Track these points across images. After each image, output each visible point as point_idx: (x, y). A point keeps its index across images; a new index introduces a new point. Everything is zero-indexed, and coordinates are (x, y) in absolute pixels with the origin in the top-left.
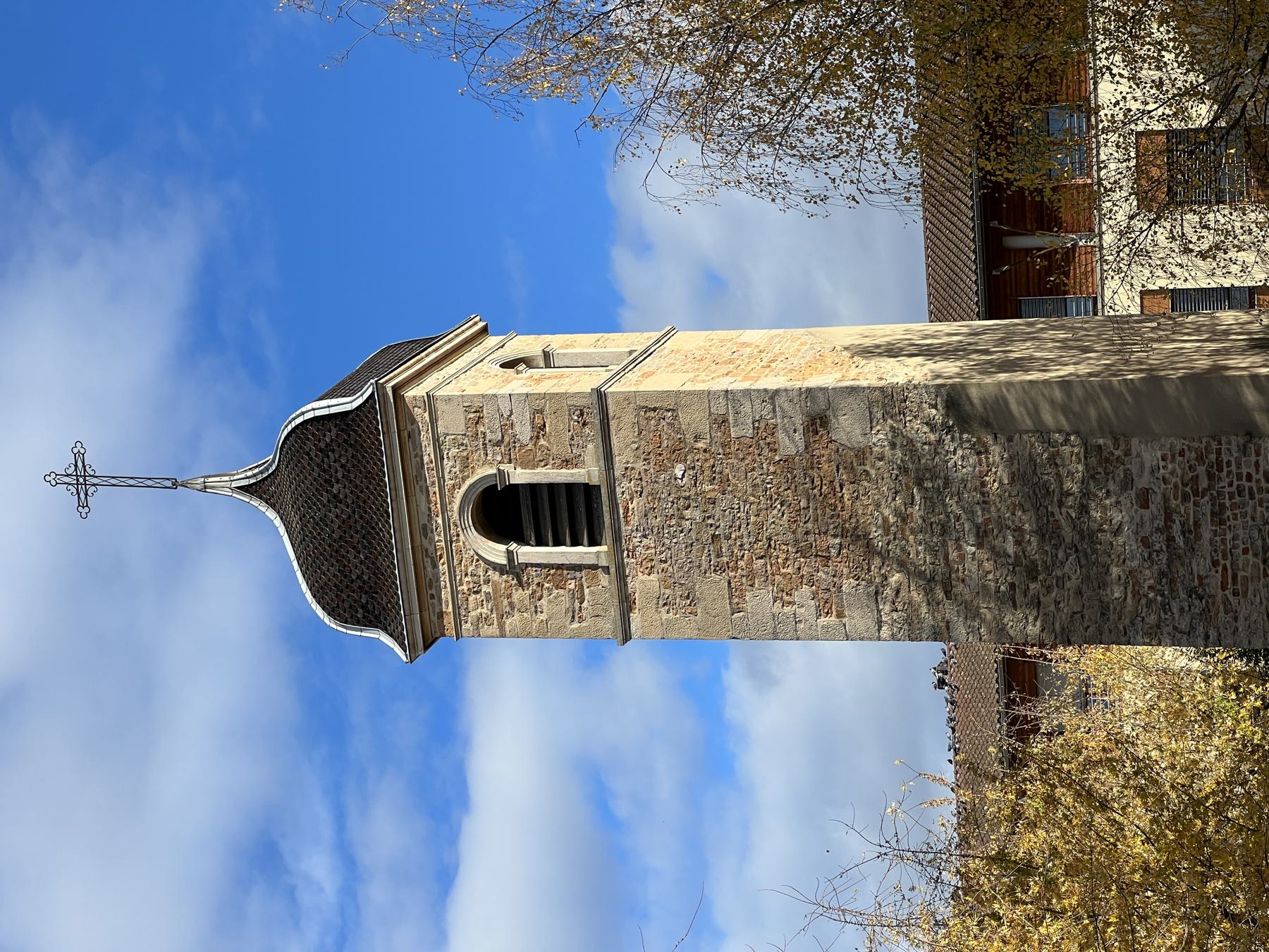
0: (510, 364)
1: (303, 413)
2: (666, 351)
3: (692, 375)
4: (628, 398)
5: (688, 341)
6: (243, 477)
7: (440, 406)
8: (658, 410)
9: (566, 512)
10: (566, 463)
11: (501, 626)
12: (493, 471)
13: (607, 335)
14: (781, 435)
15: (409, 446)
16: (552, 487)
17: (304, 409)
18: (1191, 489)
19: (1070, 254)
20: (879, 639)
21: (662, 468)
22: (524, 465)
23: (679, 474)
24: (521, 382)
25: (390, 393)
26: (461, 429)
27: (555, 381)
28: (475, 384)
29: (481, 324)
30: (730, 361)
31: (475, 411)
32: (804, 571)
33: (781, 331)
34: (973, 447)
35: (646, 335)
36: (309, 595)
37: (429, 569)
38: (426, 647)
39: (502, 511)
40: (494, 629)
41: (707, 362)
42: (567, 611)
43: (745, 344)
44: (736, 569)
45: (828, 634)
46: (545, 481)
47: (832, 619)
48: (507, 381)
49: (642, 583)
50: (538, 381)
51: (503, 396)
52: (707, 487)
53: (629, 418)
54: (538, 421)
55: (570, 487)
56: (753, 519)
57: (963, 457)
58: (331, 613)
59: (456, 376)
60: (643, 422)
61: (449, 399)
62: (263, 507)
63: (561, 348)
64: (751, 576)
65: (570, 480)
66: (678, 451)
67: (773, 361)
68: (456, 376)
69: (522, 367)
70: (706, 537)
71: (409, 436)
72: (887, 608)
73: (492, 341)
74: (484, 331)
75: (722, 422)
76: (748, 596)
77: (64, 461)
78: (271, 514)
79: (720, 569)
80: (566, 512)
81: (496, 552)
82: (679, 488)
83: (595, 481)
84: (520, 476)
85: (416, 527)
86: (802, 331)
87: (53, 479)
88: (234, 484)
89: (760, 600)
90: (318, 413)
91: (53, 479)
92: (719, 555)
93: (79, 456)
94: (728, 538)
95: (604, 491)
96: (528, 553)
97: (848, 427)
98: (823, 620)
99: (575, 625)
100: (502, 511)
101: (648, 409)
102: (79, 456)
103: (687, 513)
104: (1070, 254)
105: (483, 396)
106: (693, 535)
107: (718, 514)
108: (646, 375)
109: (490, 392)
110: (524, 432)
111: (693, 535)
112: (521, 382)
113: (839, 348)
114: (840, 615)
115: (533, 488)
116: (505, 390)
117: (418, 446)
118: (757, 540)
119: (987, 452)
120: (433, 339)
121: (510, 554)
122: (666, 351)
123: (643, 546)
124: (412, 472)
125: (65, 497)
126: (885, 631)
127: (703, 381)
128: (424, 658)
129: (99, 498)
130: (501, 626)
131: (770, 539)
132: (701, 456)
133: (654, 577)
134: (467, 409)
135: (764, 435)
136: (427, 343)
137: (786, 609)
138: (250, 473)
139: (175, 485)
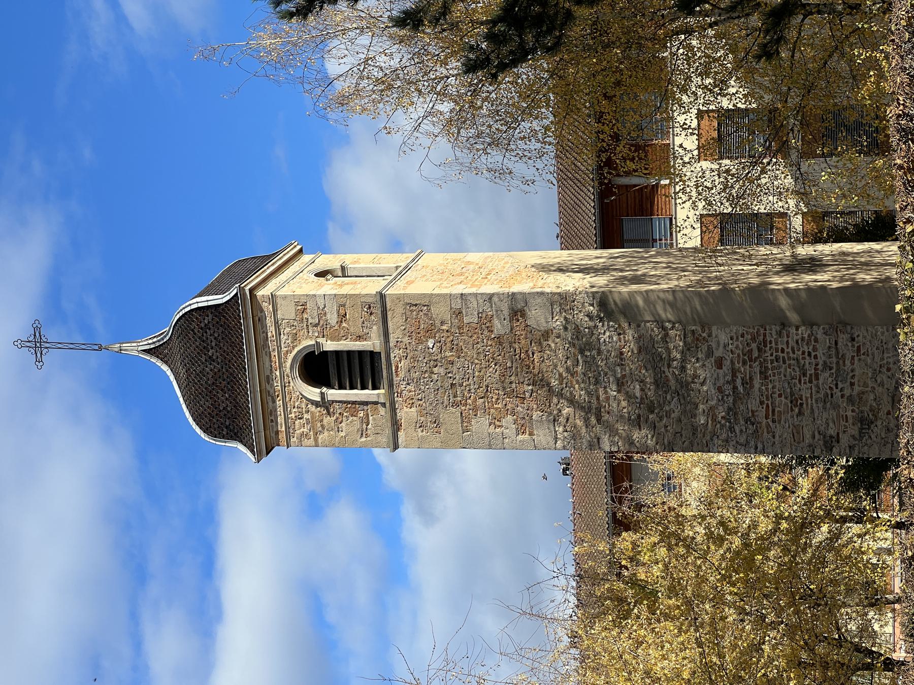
2: (419, 267)
3: (439, 283)
4: (399, 297)
5: (432, 259)
6: (146, 343)
7: (279, 301)
8: (418, 306)
9: (361, 368)
10: (359, 338)
11: (316, 440)
12: (313, 342)
15: (259, 326)
16: (349, 353)
17: (191, 302)
21: (420, 342)
27: (352, 286)
29: (299, 247)
31: (302, 306)
32: (509, 406)
33: (491, 254)
38: (268, 453)
39: (318, 368)
41: (445, 276)
42: (358, 430)
43: (469, 263)
44: (466, 405)
49: (406, 413)
50: (341, 286)
52: (448, 354)
53: (400, 310)
54: (342, 312)
55: (361, 353)
56: (477, 374)
59: (287, 282)
60: (408, 313)
61: (285, 297)
64: (475, 409)
66: (430, 331)
67: (488, 274)
71: (259, 321)
72: (561, 429)
73: (306, 258)
74: (301, 251)
78: (165, 368)
80: (361, 368)
81: (313, 393)
83: (377, 350)
84: (329, 346)
88: (140, 348)
89: (481, 424)
90: (200, 305)
94: (461, 385)
95: (383, 355)
96: (333, 394)
97: (537, 317)
99: (363, 439)
100: (318, 368)
101: (411, 305)
104: (799, 308)
105: (307, 296)
106: (439, 383)
108: (410, 283)
109: (311, 293)
110: (333, 318)
112: (330, 287)
114: (531, 434)
115: (337, 353)
119: (624, 333)
121: (322, 394)
122: (419, 267)
123: (406, 390)
125: (28, 356)
130: (316, 440)
132: (445, 334)
133: (413, 409)
136: (266, 259)
137: (498, 430)
138: (150, 341)
139: (100, 349)
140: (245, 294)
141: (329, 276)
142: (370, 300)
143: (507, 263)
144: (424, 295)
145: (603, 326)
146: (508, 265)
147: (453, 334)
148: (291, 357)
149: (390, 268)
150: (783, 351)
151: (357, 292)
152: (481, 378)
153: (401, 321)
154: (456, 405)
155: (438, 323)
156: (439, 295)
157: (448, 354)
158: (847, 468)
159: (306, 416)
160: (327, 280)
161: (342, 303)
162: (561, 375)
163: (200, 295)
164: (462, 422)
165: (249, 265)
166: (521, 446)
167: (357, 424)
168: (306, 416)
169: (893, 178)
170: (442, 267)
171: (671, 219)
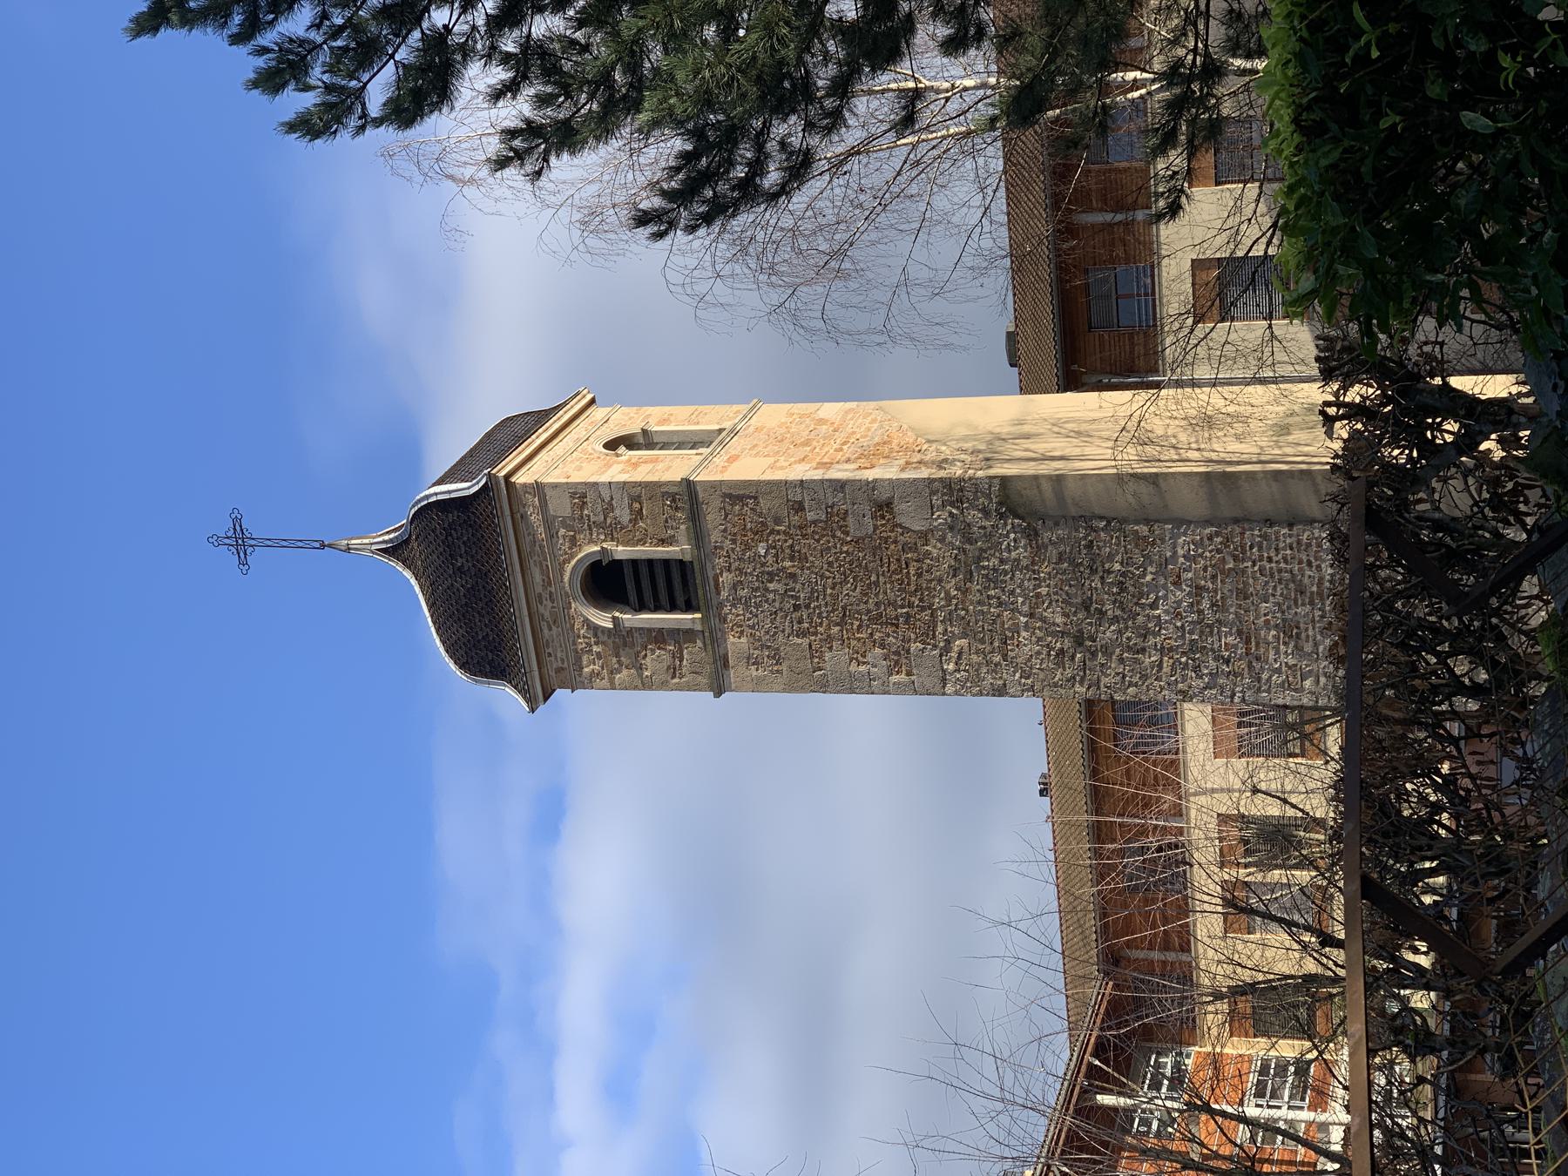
0: (612, 445)
1: (427, 497)
2: (751, 429)
3: (772, 460)
6: (386, 537)
7: (549, 492)
8: (739, 495)
9: (667, 584)
10: (662, 542)
12: (597, 548)
15: (522, 527)
18: (1219, 571)
19: (1187, 925)
21: (748, 547)
22: (626, 544)
23: (762, 552)
24: (620, 467)
26: (567, 512)
28: (579, 469)
29: (589, 397)
30: (807, 443)
31: (581, 494)
32: (877, 636)
33: (853, 405)
34: (1023, 531)
35: (735, 408)
38: (546, 699)
39: (607, 583)
41: (786, 444)
43: (821, 421)
44: (815, 634)
47: (902, 677)
49: (736, 644)
50: (635, 465)
51: (603, 484)
52: (788, 564)
53: (716, 503)
55: (666, 563)
56: (829, 591)
59: (563, 459)
61: (555, 486)
62: (400, 568)
63: (660, 423)
65: (666, 557)
66: (760, 532)
67: (845, 443)
70: (788, 606)
71: (519, 519)
72: (951, 667)
73: (598, 413)
74: (593, 401)
75: (799, 507)
76: (827, 656)
77: (224, 527)
78: (408, 574)
79: (802, 634)
80: (667, 584)
81: (603, 619)
82: (763, 565)
83: (688, 558)
84: (621, 551)
86: (873, 404)
89: (836, 658)
90: (440, 497)
91: (216, 541)
93: (237, 522)
94: (807, 607)
95: (696, 564)
96: (629, 618)
97: (911, 516)
98: (895, 678)
100: (607, 583)
101: (730, 496)
102: (237, 522)
103: (771, 586)
104: (1187, 925)
106: (777, 604)
108: (733, 459)
109: (592, 480)
111: (777, 604)
112: (620, 467)
114: (909, 674)
115: (634, 563)
116: (604, 478)
117: (529, 525)
119: (1037, 534)
120: (542, 417)
121: (614, 618)
122: (751, 429)
123: (733, 614)
124: (526, 548)
125: (229, 557)
126: (949, 688)
127: (782, 468)
128: (542, 708)
129: (257, 557)
131: (844, 608)
132: (782, 537)
133: (743, 640)
134: (573, 496)
136: (542, 417)
137: (862, 668)
138: (386, 537)
139: (323, 546)
140: (497, 483)
141: (622, 449)
143: (874, 421)
150: (1270, 560)
151: (656, 479)
152: (835, 597)
155: (770, 524)
161: (638, 494)
163: (440, 482)
164: (812, 657)
165: (518, 428)
166: (900, 689)
167: (666, 657)
168: (595, 648)
169: (1449, 275)
170: (783, 430)
171: (1152, 267)
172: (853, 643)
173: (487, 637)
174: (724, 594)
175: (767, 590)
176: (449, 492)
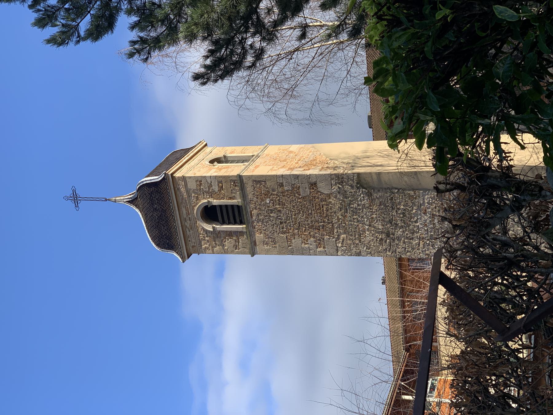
1: (143, 182)
2: (265, 155)
3: (271, 167)
4: (250, 177)
5: (273, 150)
6: (129, 197)
7: (188, 180)
8: (259, 181)
9: (233, 214)
10: (231, 198)
11: (213, 250)
12: (206, 201)
13: (246, 147)
14: (301, 190)
15: (178, 193)
16: (226, 206)
17: (142, 180)
20: (337, 255)
21: (263, 200)
23: (268, 202)
24: (214, 170)
25: (170, 176)
27: (226, 170)
28: (199, 171)
29: (205, 143)
30: (285, 160)
31: (200, 180)
32: (312, 233)
33: (303, 145)
34: (366, 194)
36: (150, 239)
37: (188, 232)
38: (188, 257)
39: (210, 213)
40: (211, 251)
41: (277, 161)
42: (234, 245)
43: (291, 152)
44: (289, 233)
45: (321, 254)
46: (224, 204)
47: (322, 249)
48: (210, 170)
49: (259, 237)
50: (220, 169)
51: (208, 177)
52: (278, 206)
53: (250, 183)
54: (221, 185)
55: (232, 206)
56: (293, 217)
57: (363, 197)
58: (157, 245)
60: (255, 185)
61: (190, 177)
62: (134, 208)
64: (294, 235)
66: (267, 194)
67: (299, 160)
68: (193, 167)
69: (216, 163)
71: (177, 190)
72: (340, 245)
74: (206, 145)
76: (293, 241)
77: (69, 193)
78: (137, 210)
80: (233, 214)
81: (209, 227)
82: (268, 207)
83: (240, 204)
84: (215, 202)
85: (182, 219)
87: (67, 198)
88: (125, 200)
89: (296, 242)
90: (147, 182)
91: (67, 198)
92: (283, 228)
93: (74, 191)
94: (285, 222)
95: (243, 206)
96: (219, 227)
97: (324, 188)
98: (319, 249)
99: (237, 250)
100: (210, 213)
101: (255, 181)
103: (272, 215)
105: (202, 177)
106: (274, 222)
107: (282, 215)
108: (257, 167)
109: (204, 175)
110: (216, 189)
111: (274, 222)
112: (214, 170)
113: (322, 154)
114: (324, 248)
115: (220, 206)
118: (295, 224)
121: (213, 227)
122: (265, 155)
123: (258, 225)
124: (180, 201)
125: (71, 204)
126: (339, 253)
127: (275, 170)
128: (187, 261)
129: (82, 204)
130: (213, 250)
131: (299, 223)
132: (275, 196)
134: (197, 181)
135: (295, 190)
136: (187, 151)
137: (306, 246)
138: (129, 197)
139: (106, 200)
140: (168, 176)
142: (235, 179)
143: (310, 152)
144: (262, 176)
145: (359, 191)
146: (311, 154)
147: (279, 196)
148: (196, 208)
149: (249, 156)
151: (227, 175)
152: (296, 219)
153: (252, 189)
154: (284, 233)
156: (270, 176)
157: (278, 206)
158: (494, 228)
159: (206, 238)
160: (214, 166)
161: (221, 180)
162: (338, 217)
164: (288, 241)
165: (178, 155)
168: (206, 238)
172: (303, 236)
173: (166, 233)
174: (254, 218)
175: (270, 216)
176: (151, 180)
